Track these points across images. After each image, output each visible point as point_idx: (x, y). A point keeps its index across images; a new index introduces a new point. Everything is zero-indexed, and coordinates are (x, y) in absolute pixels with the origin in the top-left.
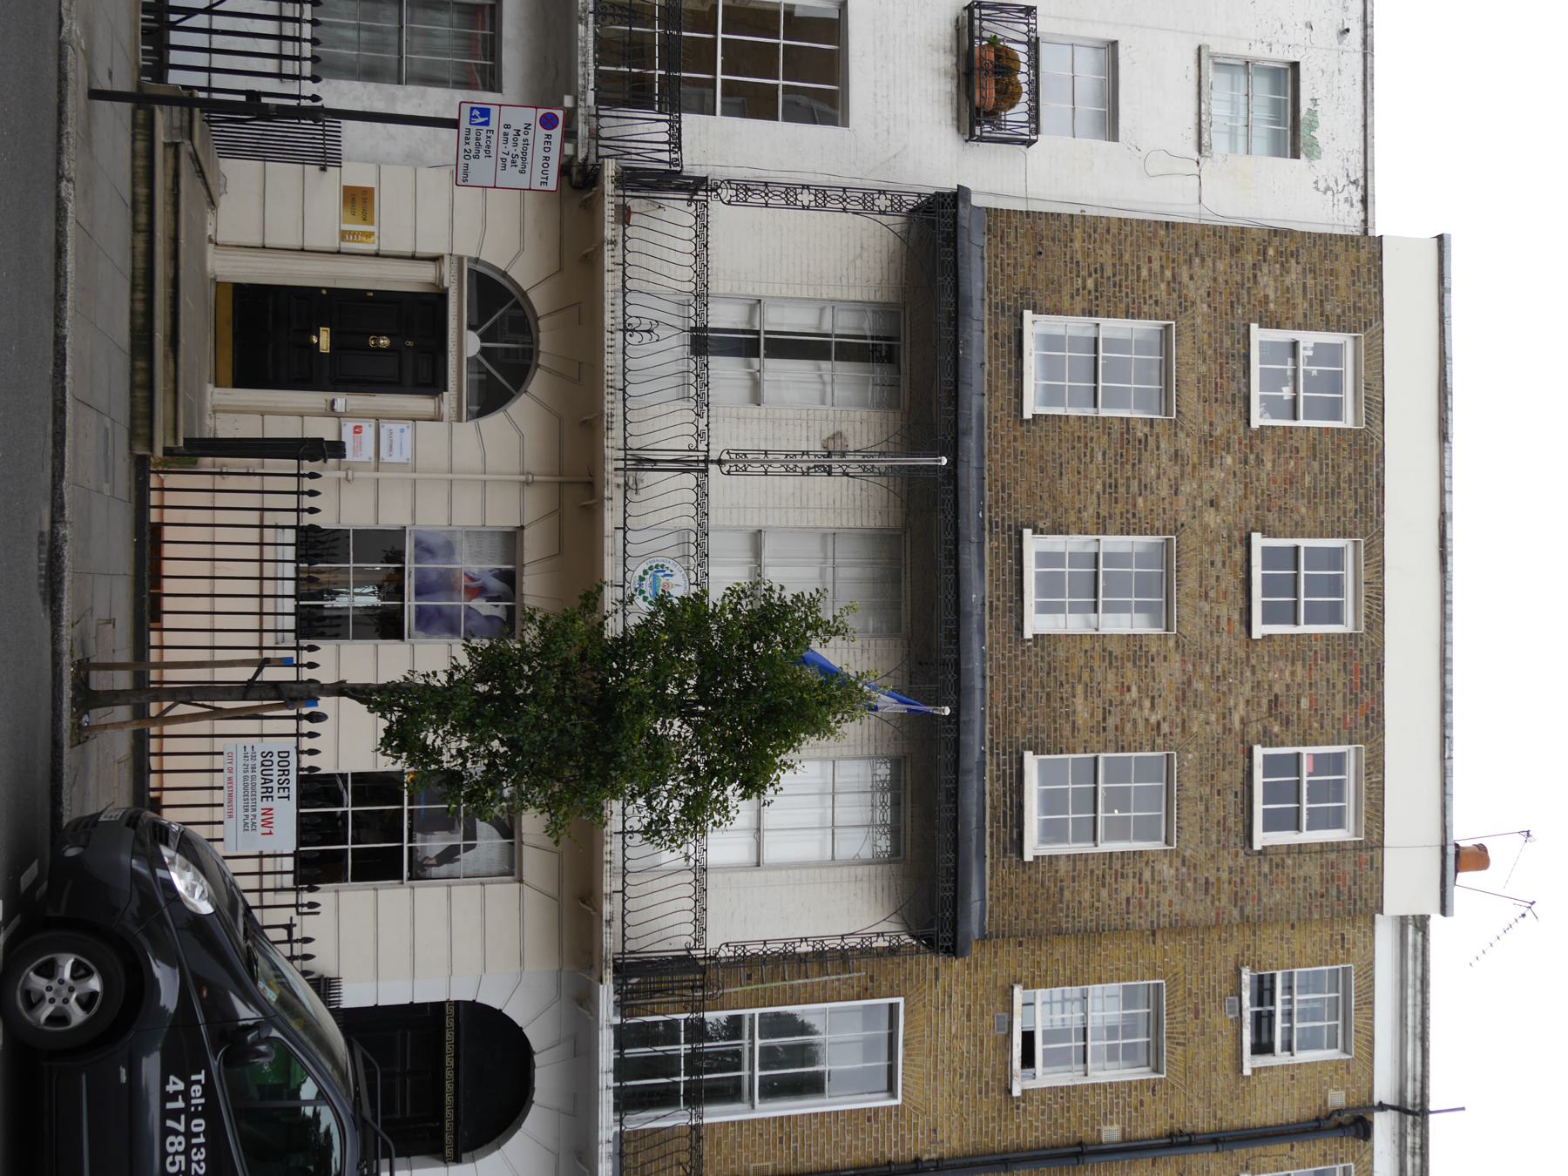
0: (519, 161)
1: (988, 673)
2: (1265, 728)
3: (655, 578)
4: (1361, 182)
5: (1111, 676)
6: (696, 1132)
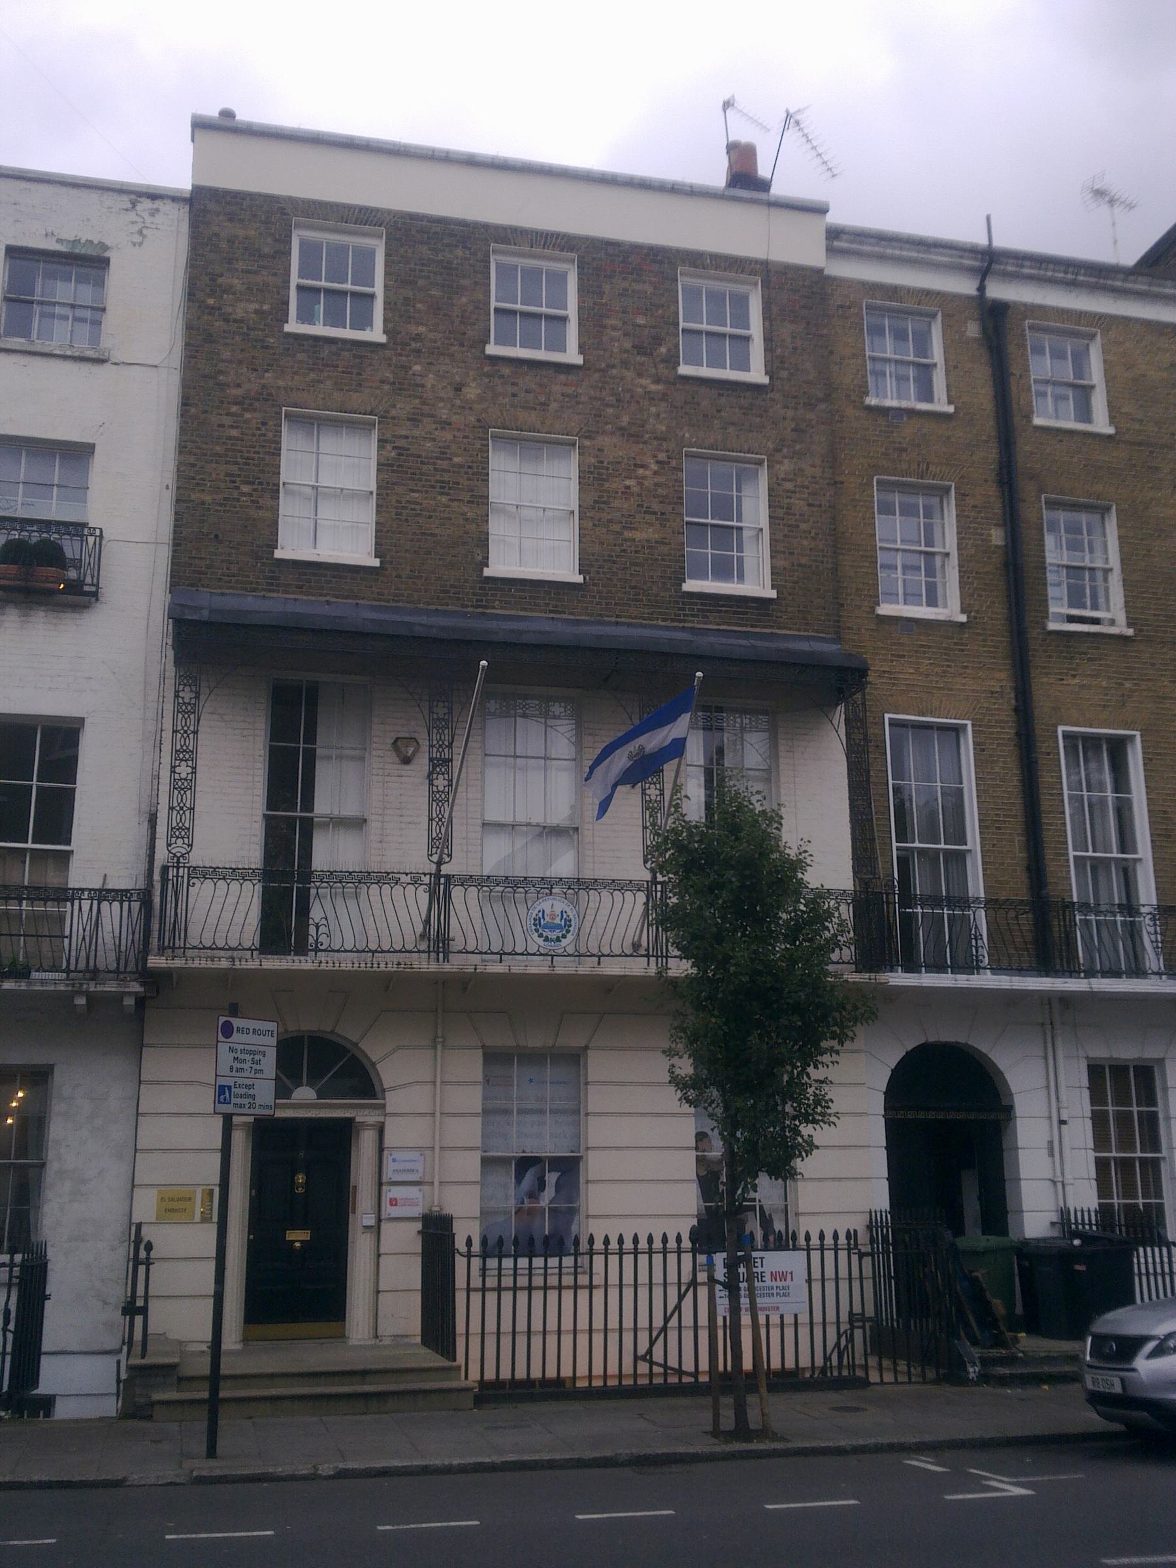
0: (257, 1057)
1: (613, 619)
2: (662, 361)
3: (545, 927)
4: (133, 197)
5: (616, 503)
6: (992, 904)
